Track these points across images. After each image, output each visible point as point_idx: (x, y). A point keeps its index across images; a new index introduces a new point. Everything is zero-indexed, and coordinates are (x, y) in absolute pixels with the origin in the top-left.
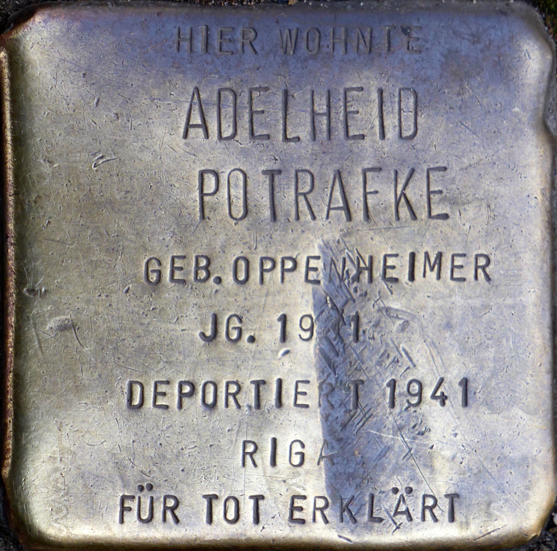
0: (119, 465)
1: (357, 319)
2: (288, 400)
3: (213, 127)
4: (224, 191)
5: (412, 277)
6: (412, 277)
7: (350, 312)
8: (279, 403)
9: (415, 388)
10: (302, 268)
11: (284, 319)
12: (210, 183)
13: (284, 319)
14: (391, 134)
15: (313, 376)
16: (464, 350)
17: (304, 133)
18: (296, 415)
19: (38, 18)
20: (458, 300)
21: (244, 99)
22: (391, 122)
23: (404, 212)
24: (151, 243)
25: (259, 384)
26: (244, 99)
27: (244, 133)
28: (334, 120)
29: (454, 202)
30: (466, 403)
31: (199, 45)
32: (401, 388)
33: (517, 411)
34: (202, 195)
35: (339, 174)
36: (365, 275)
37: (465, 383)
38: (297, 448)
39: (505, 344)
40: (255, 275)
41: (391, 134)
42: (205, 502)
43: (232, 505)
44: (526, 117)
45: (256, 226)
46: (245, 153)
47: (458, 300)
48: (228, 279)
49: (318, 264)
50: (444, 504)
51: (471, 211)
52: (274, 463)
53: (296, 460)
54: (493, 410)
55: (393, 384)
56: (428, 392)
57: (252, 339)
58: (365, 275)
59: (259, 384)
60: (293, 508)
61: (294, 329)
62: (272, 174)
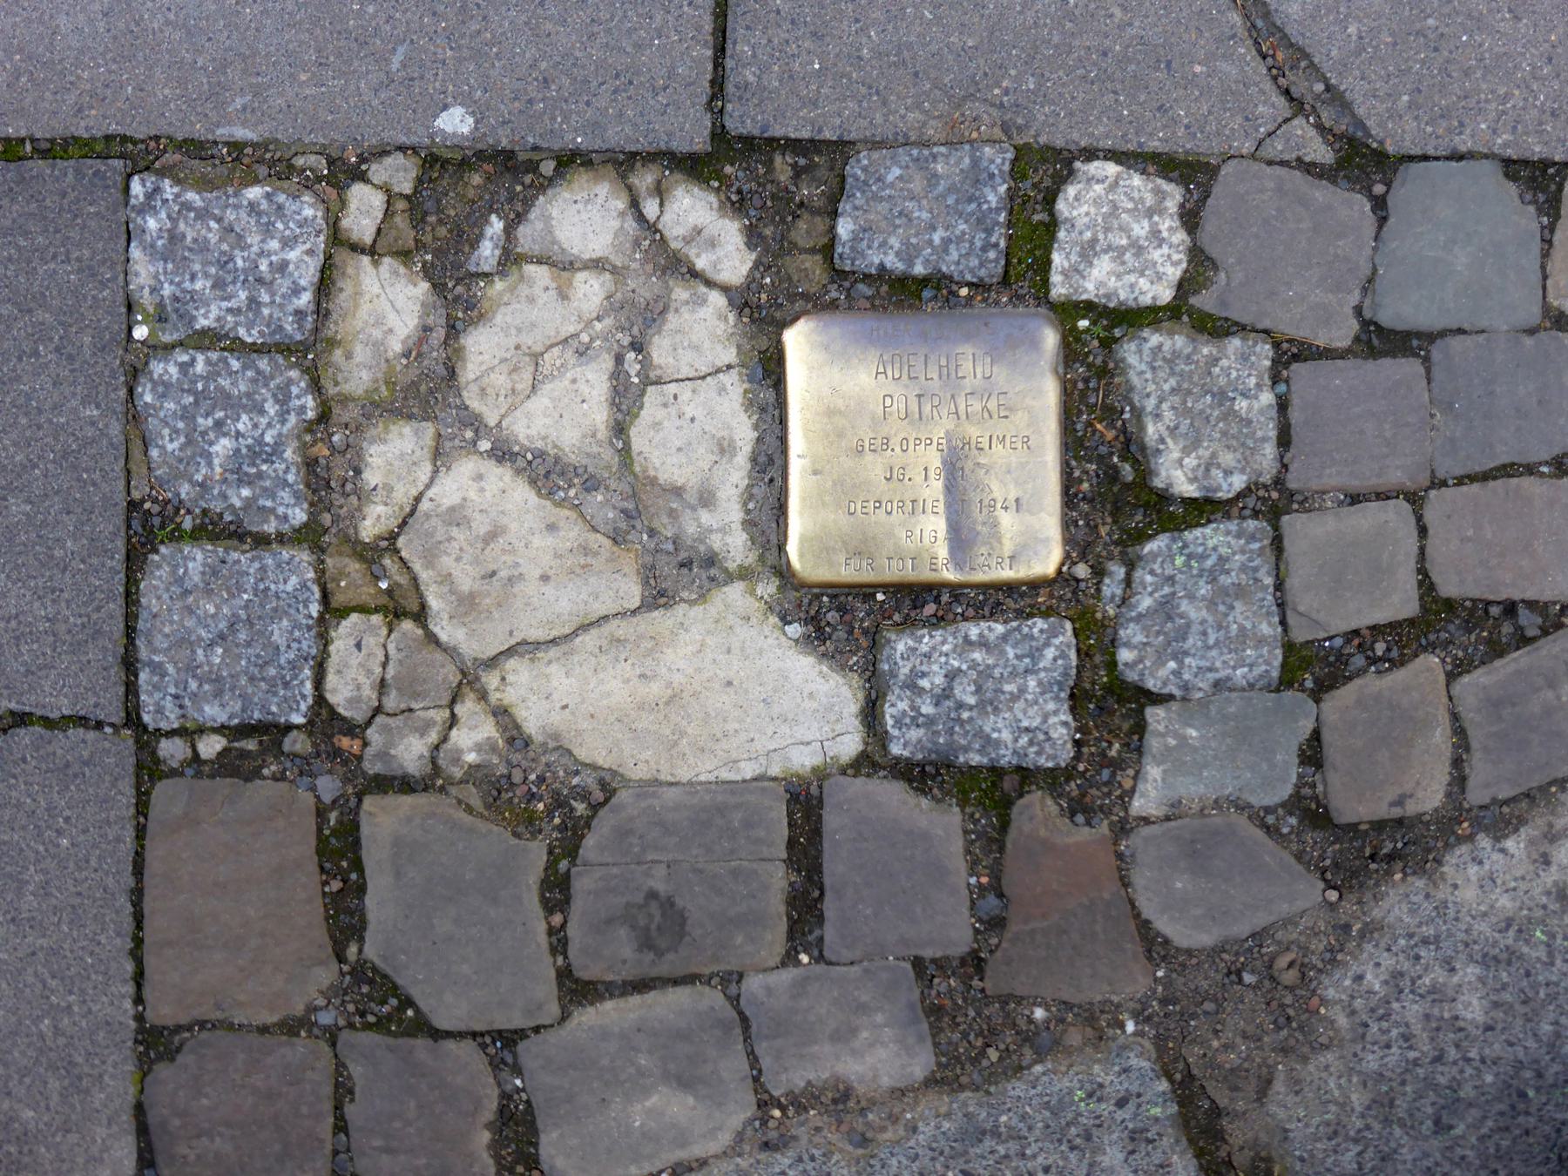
0: (844, 542)
3: (890, 373)
7: (959, 465)
14: (979, 375)
15: (941, 498)
16: (1016, 483)
17: (936, 377)
18: (933, 518)
20: (1014, 459)
21: (905, 359)
22: (979, 371)
23: (986, 415)
26: (905, 359)
27: (905, 376)
28: (1075, 136)
29: (1011, 409)
32: (986, 502)
33: (1043, 515)
37: (1017, 500)
39: (619, 295)
40: (911, 446)
41: (979, 375)
44: (1047, 367)
45: (912, 423)
46: (906, 386)
47: (1014, 459)
48: (898, 449)
51: (1020, 413)
54: (1032, 514)
56: (999, 505)
59: (913, 501)
61: (932, 474)
62: (919, 396)
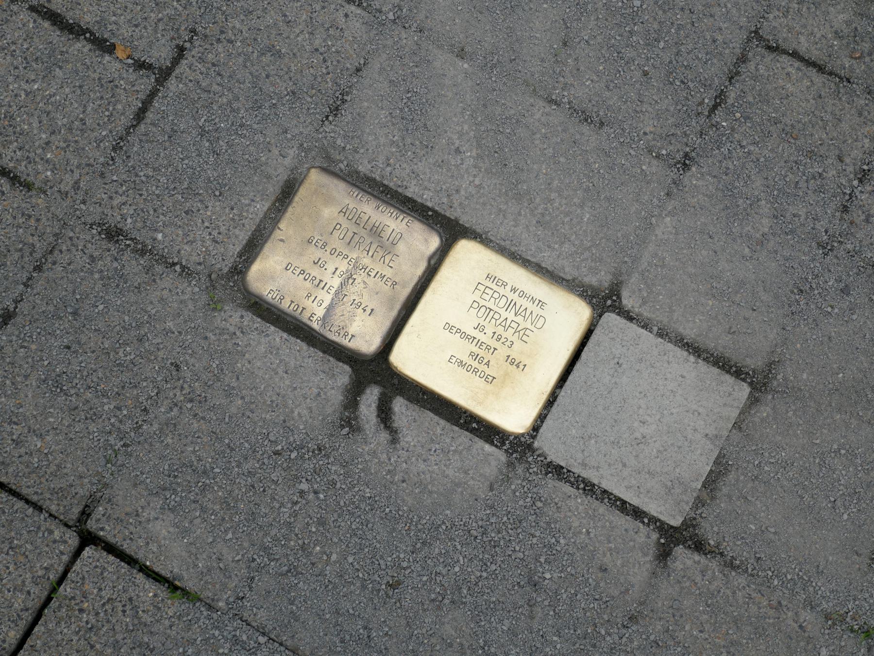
1: (355, 279)
2: (326, 288)
4: (340, 231)
5: (375, 277)
6: (375, 277)
7: (354, 276)
8: (323, 288)
9: (359, 304)
10: (349, 259)
11: (336, 269)
12: (338, 226)
13: (336, 269)
19: (393, 405)
24: (351, 286)
25: (321, 281)
30: (369, 315)
31: (355, 195)
34: (335, 228)
35: (371, 243)
36: (363, 270)
38: (321, 302)
42: (754, 363)
43: (296, 307)
48: (329, 251)
49: (353, 261)
50: (350, 336)
52: (313, 302)
53: (319, 304)
55: (354, 300)
57: (326, 269)
58: (363, 270)
60: (311, 316)
61: (338, 272)
